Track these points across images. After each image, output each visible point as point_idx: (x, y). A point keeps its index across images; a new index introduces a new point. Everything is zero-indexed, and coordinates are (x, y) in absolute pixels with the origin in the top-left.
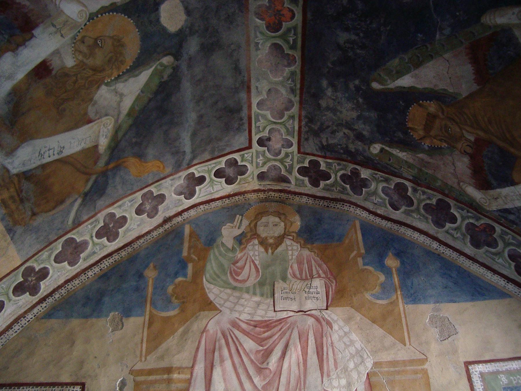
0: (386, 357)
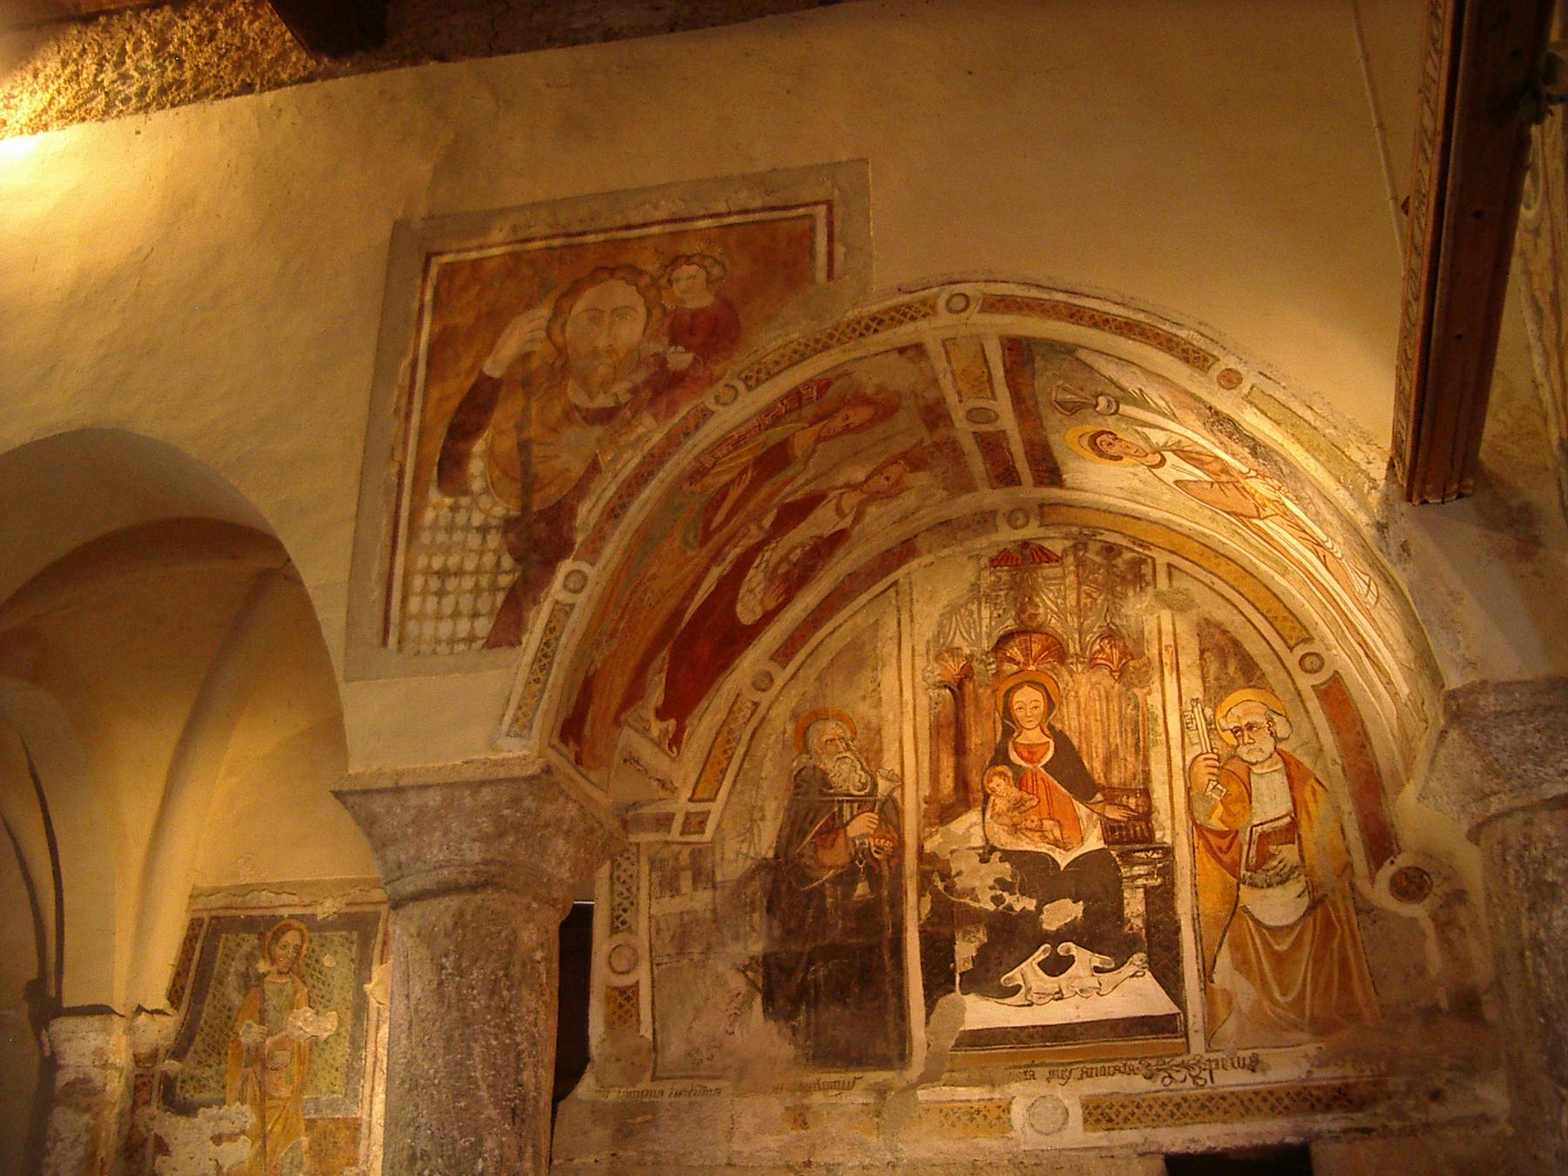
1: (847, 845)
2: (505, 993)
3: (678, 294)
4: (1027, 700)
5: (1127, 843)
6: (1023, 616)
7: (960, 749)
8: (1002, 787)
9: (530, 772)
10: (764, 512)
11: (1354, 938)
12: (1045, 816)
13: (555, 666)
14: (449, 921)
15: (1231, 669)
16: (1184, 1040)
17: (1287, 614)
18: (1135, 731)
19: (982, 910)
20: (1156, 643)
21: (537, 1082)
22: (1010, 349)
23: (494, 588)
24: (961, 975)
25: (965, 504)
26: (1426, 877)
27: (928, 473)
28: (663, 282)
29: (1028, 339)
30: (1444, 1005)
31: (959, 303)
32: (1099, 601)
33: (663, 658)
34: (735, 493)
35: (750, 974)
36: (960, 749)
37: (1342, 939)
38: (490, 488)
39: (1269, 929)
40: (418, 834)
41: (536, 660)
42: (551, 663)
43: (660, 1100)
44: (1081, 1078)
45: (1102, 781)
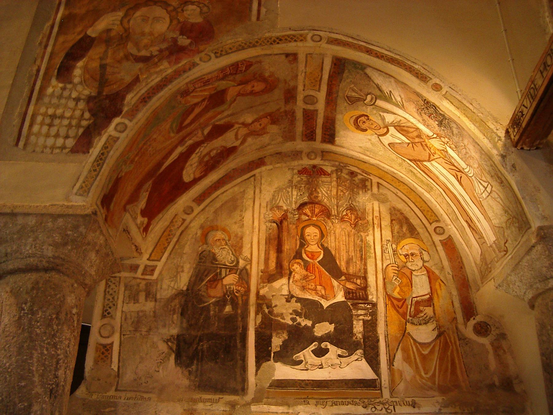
1: (222, 288)
2: (55, 327)
3: (186, 16)
4: (312, 232)
5: (355, 299)
6: (311, 196)
7: (279, 250)
8: (298, 269)
9: (86, 213)
10: (206, 126)
11: (457, 350)
12: (318, 283)
13: (105, 165)
14: (30, 286)
15: (404, 229)
16: (379, 391)
17: (429, 209)
18: (361, 251)
19: (286, 324)
20: (371, 214)
21: (66, 377)
22: (335, 64)
23: (78, 126)
24: (274, 353)
25: (289, 146)
26: (488, 326)
27: (278, 127)
28: (179, 10)
29: (345, 59)
30: (497, 383)
31: (318, 38)
32: (346, 194)
33: (149, 185)
34: (197, 111)
35: (170, 343)
36: (279, 250)
37: (452, 352)
38: (83, 82)
39: (420, 344)
40: (19, 239)
41: (96, 160)
42: (103, 164)
43: (119, 400)
44: (332, 406)
45: (345, 271)
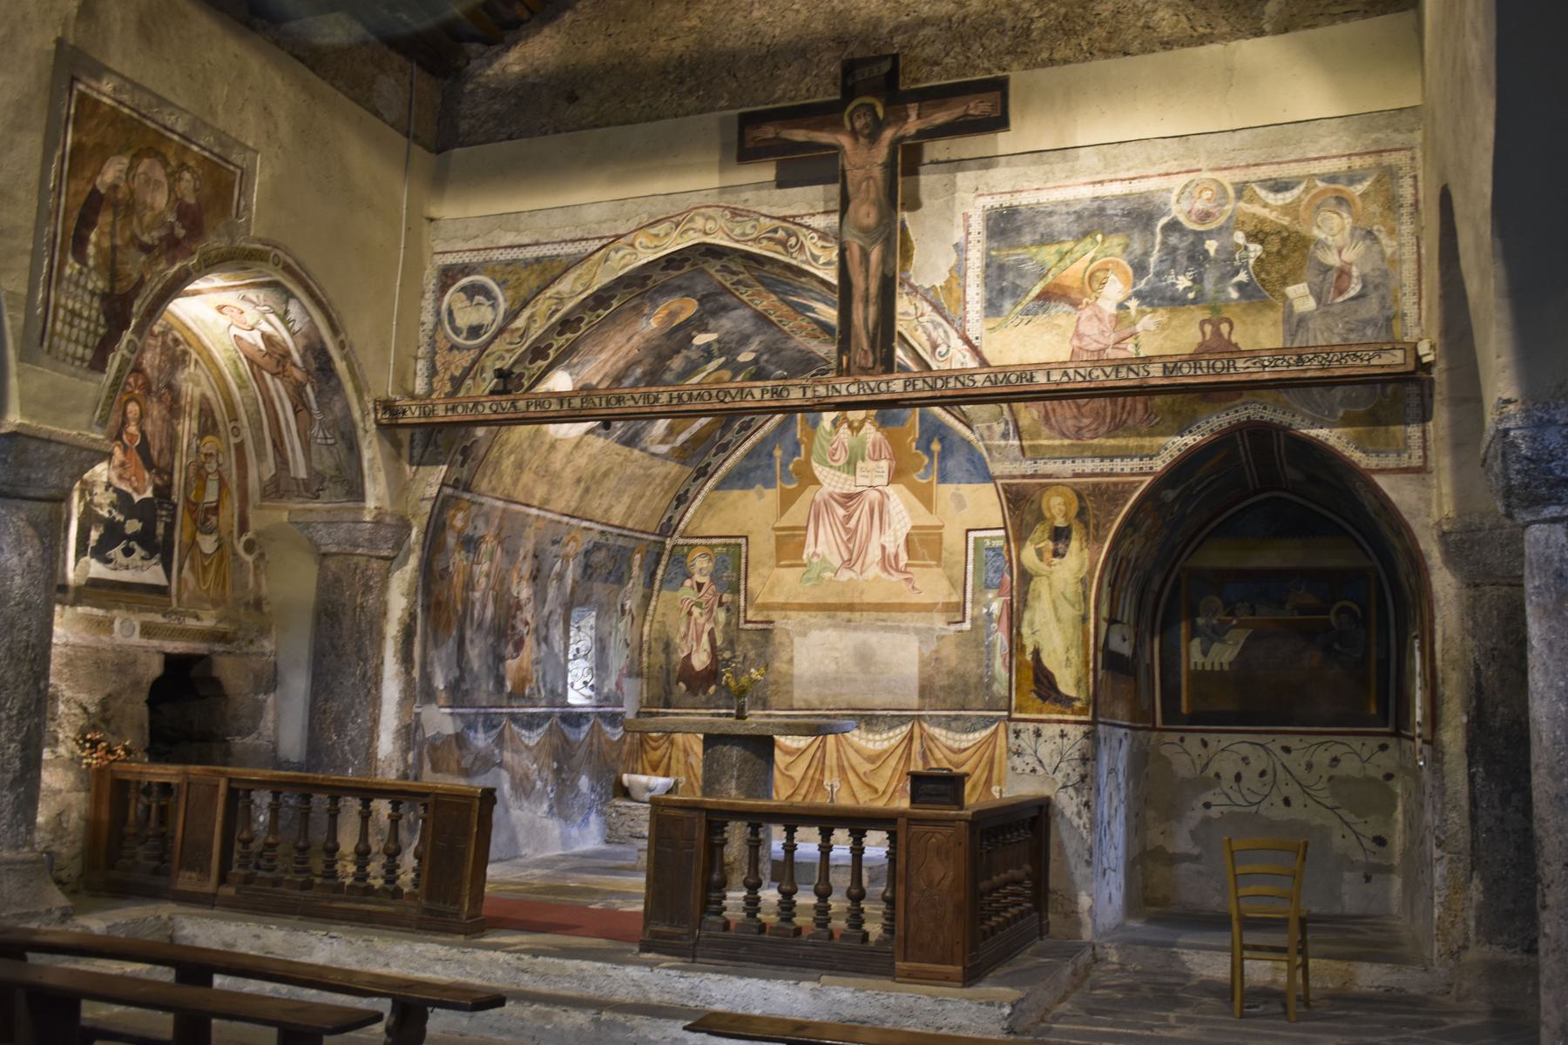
0: (920, 522)
41: (112, 386)
